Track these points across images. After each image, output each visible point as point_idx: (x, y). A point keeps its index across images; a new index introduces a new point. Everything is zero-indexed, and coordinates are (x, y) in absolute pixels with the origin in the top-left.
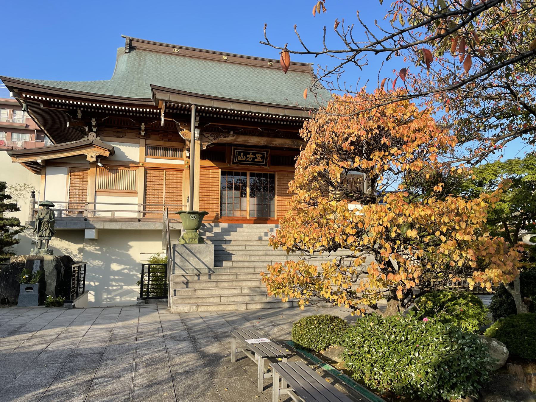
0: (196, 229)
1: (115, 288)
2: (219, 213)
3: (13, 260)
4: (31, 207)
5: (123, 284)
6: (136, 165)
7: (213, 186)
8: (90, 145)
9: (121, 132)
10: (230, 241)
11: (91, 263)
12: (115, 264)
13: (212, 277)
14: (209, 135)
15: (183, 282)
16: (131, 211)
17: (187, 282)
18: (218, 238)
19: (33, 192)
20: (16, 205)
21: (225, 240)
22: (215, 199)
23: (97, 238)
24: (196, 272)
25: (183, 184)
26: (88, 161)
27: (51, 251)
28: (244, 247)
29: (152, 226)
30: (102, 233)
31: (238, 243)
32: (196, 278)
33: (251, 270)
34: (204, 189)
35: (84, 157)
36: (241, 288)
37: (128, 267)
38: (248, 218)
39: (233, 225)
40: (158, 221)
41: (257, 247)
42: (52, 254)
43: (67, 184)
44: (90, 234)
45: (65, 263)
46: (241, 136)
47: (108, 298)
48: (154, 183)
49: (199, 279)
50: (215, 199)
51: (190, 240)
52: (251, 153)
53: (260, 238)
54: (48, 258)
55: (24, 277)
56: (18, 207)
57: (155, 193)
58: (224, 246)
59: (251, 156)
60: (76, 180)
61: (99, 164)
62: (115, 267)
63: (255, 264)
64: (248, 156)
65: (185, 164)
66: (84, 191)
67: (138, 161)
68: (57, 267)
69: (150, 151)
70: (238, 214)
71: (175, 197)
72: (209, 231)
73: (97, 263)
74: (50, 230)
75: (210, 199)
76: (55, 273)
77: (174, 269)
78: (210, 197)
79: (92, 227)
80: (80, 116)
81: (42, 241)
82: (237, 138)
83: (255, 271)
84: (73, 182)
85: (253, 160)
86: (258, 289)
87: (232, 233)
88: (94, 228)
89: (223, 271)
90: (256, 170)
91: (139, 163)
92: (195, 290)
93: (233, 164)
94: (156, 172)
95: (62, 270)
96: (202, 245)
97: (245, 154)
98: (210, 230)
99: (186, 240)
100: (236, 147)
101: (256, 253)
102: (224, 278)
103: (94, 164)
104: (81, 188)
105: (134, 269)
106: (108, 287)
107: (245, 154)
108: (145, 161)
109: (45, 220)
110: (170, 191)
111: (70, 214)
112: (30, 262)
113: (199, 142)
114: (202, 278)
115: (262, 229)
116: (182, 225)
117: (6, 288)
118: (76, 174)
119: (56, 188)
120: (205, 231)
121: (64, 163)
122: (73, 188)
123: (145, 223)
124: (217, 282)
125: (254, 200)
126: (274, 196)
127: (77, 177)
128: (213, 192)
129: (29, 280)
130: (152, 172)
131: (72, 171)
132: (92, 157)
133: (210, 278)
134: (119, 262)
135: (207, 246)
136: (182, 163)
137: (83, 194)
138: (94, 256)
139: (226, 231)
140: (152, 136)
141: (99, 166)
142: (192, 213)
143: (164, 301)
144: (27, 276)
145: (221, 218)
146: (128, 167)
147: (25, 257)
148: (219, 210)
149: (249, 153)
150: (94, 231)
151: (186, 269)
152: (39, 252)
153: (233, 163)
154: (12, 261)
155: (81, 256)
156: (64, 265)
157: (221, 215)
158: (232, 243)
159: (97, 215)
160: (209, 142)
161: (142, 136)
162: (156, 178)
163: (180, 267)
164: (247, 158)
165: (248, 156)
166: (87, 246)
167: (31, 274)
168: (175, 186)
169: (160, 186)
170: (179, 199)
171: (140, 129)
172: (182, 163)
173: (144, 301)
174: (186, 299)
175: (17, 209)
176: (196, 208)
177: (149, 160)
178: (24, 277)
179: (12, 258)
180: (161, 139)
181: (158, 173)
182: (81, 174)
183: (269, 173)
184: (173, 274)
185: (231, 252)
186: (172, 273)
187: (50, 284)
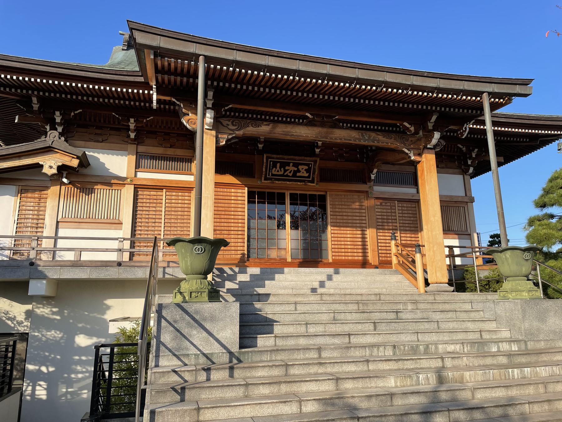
0: (205, 274)
1: (80, 376)
2: (246, 252)
6: (121, 181)
7: (236, 213)
8: (48, 150)
9: (101, 134)
10: (268, 295)
11: (43, 335)
12: (82, 336)
13: (237, 373)
14: (230, 123)
15: (173, 389)
16: (107, 250)
17: (183, 389)
18: (244, 292)
21: (259, 294)
22: (240, 233)
23: (52, 295)
24: (202, 360)
26: (45, 174)
28: (292, 307)
30: (64, 286)
31: (281, 299)
32: (203, 376)
33: (313, 355)
34: (220, 205)
35: (39, 166)
36: (300, 402)
38: (289, 260)
39: (269, 270)
41: (316, 308)
44: (37, 287)
46: (280, 125)
47: (67, 392)
48: (147, 209)
49: (208, 379)
50: (240, 233)
51: (194, 295)
52: (291, 164)
53: (314, 290)
57: (150, 224)
58: (258, 305)
59: (291, 168)
60: (29, 204)
61: (65, 180)
63: (320, 341)
64: (287, 168)
66: (40, 221)
69: (145, 162)
70: (273, 254)
71: (179, 228)
72: (230, 280)
73: (54, 334)
75: (232, 232)
77: (157, 356)
78: (232, 228)
79: (42, 276)
80: (36, 107)
82: (274, 128)
83: (320, 357)
84: (24, 208)
85: (294, 175)
86: (337, 401)
87: (267, 282)
88: (44, 277)
89: (257, 358)
90: (299, 188)
91: (125, 179)
92: (199, 409)
94: (152, 193)
96: (215, 305)
97: (284, 165)
98: (232, 278)
99: (185, 294)
100: (269, 155)
101: (316, 318)
102: (261, 373)
103: (56, 179)
104: (35, 217)
106: (69, 374)
107: (284, 165)
108: (136, 176)
110: (173, 221)
111: (15, 257)
113: (214, 133)
114: (215, 375)
115: (312, 276)
116: (179, 264)
118: (29, 195)
120: (224, 280)
122: (23, 217)
123: (128, 269)
124: (247, 385)
125: (298, 234)
126: (327, 225)
127: (31, 199)
128: (236, 221)
130: (145, 193)
131: (22, 191)
132: (51, 167)
133: (231, 376)
135: (225, 307)
137: (39, 226)
139: (258, 280)
141: (64, 184)
142: (199, 241)
145: (248, 260)
146: (110, 184)
148: (246, 248)
150: (45, 282)
151: (184, 355)
153: (266, 179)
157: (249, 256)
158: (271, 299)
159: (58, 258)
160: (230, 134)
161: (132, 140)
163: (170, 350)
164: (285, 171)
166: (39, 308)
168: (179, 213)
169: (158, 213)
171: (128, 129)
176: (207, 232)
177: (140, 175)
180: (161, 145)
182: (36, 195)
183: (317, 193)
184: (157, 366)
185: (270, 316)
186: (152, 363)
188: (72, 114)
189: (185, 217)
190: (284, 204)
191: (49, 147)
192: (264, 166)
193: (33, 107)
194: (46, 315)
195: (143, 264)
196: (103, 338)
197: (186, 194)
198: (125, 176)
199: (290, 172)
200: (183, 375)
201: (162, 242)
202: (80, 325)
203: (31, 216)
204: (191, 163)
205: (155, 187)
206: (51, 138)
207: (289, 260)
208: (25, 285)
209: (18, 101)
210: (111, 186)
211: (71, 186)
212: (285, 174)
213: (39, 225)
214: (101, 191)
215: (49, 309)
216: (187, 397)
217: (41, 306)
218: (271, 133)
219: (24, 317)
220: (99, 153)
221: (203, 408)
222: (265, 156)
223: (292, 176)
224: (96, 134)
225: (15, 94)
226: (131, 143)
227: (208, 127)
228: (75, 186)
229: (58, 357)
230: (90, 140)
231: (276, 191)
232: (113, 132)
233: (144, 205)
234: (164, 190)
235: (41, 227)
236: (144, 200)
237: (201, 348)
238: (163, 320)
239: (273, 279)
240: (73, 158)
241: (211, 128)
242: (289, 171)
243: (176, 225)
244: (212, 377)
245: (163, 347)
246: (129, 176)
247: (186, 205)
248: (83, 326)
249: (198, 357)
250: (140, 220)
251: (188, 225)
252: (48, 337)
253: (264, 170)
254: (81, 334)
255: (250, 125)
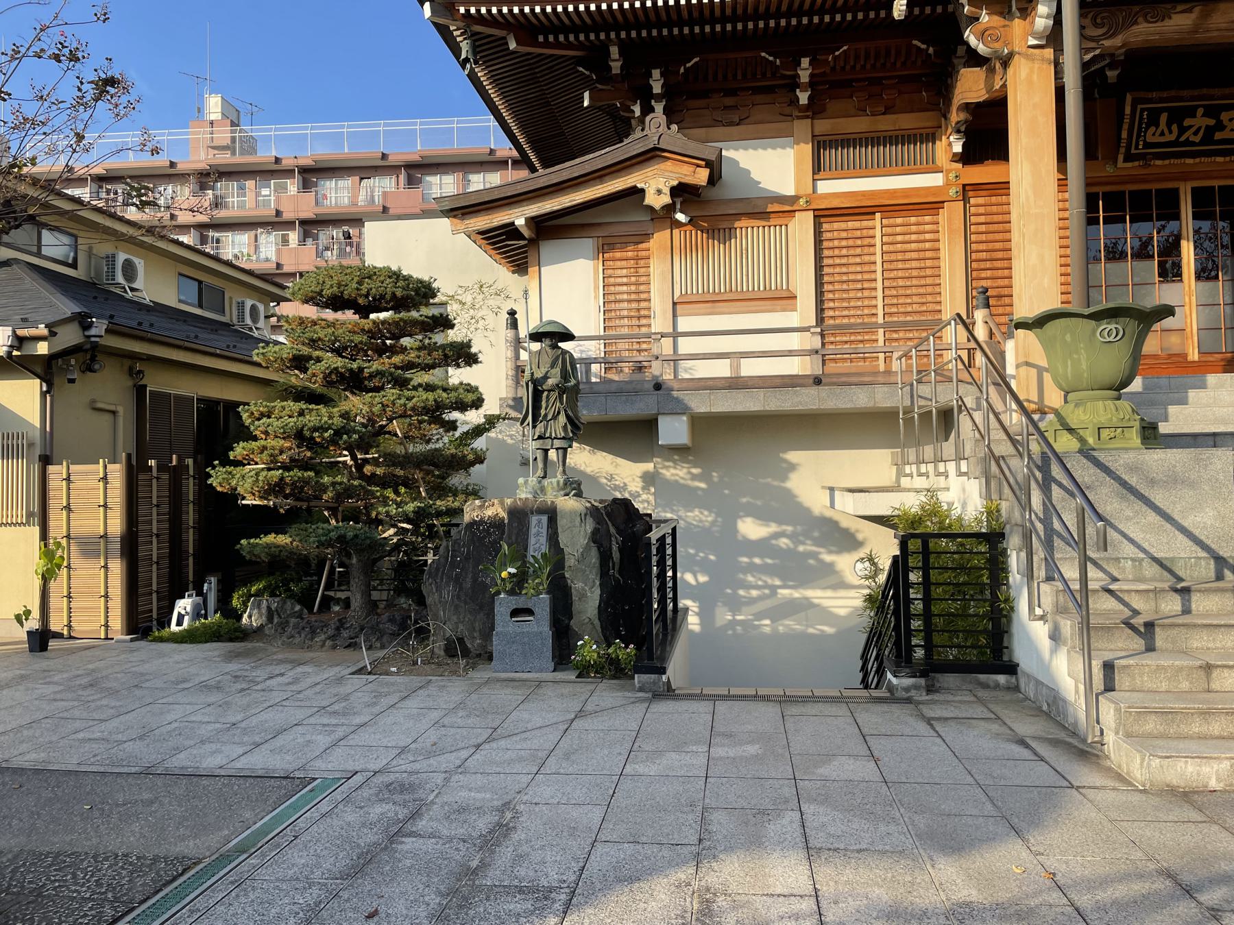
1: (754, 593)
3: (472, 511)
4: (510, 354)
5: (778, 583)
8: (652, 155)
9: (735, 107)
11: (680, 517)
12: (749, 520)
19: (512, 313)
20: (468, 345)
25: (944, 254)
27: (574, 486)
29: (860, 399)
30: (704, 425)
32: (1173, 604)
35: (636, 193)
37: (789, 529)
38: (1194, 355)
40: (881, 379)
42: (579, 495)
43: (596, 288)
44: (673, 430)
45: (621, 524)
49: (1186, 611)
51: (1105, 434)
52: (1200, 111)
54: (568, 504)
55: (504, 574)
56: (473, 350)
60: (619, 272)
61: (681, 217)
62: (750, 529)
65: (948, 184)
66: (643, 304)
67: (790, 191)
68: (598, 538)
69: (829, 155)
71: (915, 299)
74: (567, 416)
76: (594, 557)
79: (679, 409)
80: (616, 67)
81: (546, 451)
84: (612, 280)
85: (1208, 137)
91: (794, 199)
92: (1208, 668)
93: (1125, 161)
94: (851, 225)
95: (615, 548)
97: (1177, 117)
103: (664, 217)
104: (633, 297)
105: (807, 534)
107: (1177, 117)
109: (550, 382)
110: (901, 283)
112: (519, 515)
117: (456, 607)
118: (618, 255)
119: (569, 290)
121: (583, 226)
122: (612, 298)
123: (838, 389)
129: (519, 582)
130: (836, 226)
131: (605, 247)
132: (659, 192)
134: (762, 516)
136: (936, 180)
137: (642, 315)
138: (687, 496)
140: (832, 106)
141: (679, 224)
143: (997, 686)
144: (513, 570)
146: (763, 215)
147: (502, 503)
149: (1192, 113)
150: (685, 418)
152: (543, 489)
154: (467, 518)
155: (651, 498)
156: (619, 532)
162: (851, 243)
164: (1182, 130)
165: (1186, 123)
166: (667, 468)
167: (525, 562)
168: (914, 264)
169: (866, 268)
170: (931, 307)
171: (794, 84)
172: (936, 180)
173: (922, 681)
174: (1186, 715)
175: (472, 360)
177: (825, 187)
178: (504, 574)
179: (467, 508)
180: (861, 111)
181: (857, 224)
187: (583, 596)
188: (682, 70)
189: (929, 272)
190: (1177, 217)
191: (655, 149)
192: (1125, 126)
193: (610, 68)
194: (682, 481)
195: (866, 379)
196: (787, 524)
197: (927, 219)
198: (793, 194)
199: (1196, 133)
200: (1126, 599)
201: (881, 331)
202: (744, 500)
203: (625, 297)
204: (934, 143)
205: (857, 211)
206: (654, 130)
207: (1194, 355)
208: (649, 426)
209: (579, 61)
210: (768, 219)
211: (690, 227)
212: (1182, 139)
213: (642, 313)
214: (750, 234)
215: (685, 470)
216: (1159, 643)
217: (670, 464)
218: (1196, 32)
219: (641, 484)
220: (736, 149)
221: (1218, 666)
222: (1129, 98)
223: (1201, 143)
224: (726, 108)
225: (580, 46)
226: (799, 118)
227: (1035, 42)
228: (697, 227)
229: (712, 557)
230: (717, 123)
231: (1154, 186)
232: (759, 98)
233: (837, 252)
234: (878, 215)
235: (645, 317)
236: (836, 243)
237: (1146, 545)
238: (1054, 487)
239: (1183, 401)
240: (698, 166)
241: (1043, 42)
242: (1193, 129)
243: (908, 292)
244: (1193, 606)
245: (1060, 541)
246: (801, 193)
247: (927, 245)
248: (748, 503)
249: (1140, 564)
250: (831, 287)
251: (937, 289)
252: (689, 520)
253: (1124, 135)
254: (747, 515)
255: (1140, 19)
